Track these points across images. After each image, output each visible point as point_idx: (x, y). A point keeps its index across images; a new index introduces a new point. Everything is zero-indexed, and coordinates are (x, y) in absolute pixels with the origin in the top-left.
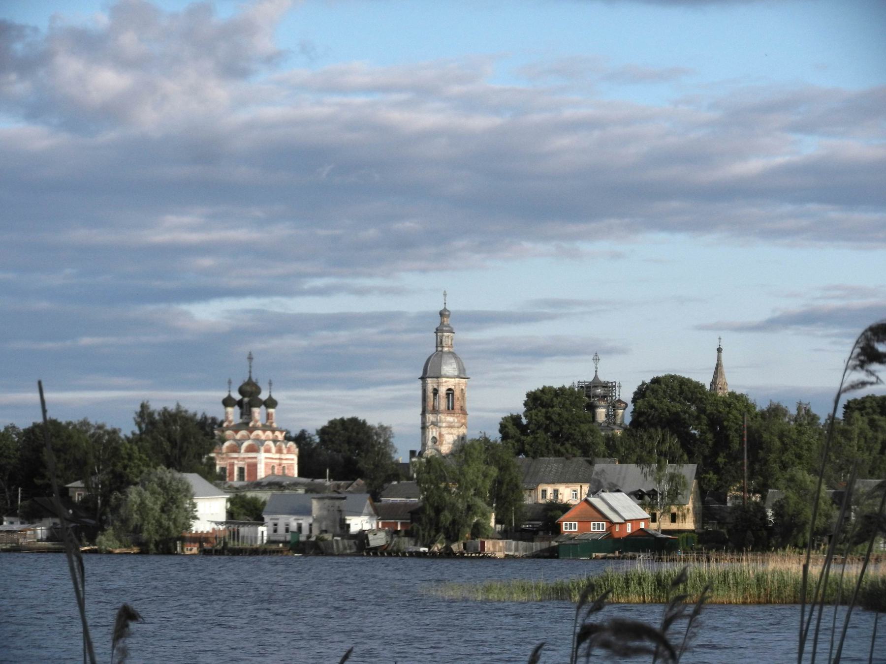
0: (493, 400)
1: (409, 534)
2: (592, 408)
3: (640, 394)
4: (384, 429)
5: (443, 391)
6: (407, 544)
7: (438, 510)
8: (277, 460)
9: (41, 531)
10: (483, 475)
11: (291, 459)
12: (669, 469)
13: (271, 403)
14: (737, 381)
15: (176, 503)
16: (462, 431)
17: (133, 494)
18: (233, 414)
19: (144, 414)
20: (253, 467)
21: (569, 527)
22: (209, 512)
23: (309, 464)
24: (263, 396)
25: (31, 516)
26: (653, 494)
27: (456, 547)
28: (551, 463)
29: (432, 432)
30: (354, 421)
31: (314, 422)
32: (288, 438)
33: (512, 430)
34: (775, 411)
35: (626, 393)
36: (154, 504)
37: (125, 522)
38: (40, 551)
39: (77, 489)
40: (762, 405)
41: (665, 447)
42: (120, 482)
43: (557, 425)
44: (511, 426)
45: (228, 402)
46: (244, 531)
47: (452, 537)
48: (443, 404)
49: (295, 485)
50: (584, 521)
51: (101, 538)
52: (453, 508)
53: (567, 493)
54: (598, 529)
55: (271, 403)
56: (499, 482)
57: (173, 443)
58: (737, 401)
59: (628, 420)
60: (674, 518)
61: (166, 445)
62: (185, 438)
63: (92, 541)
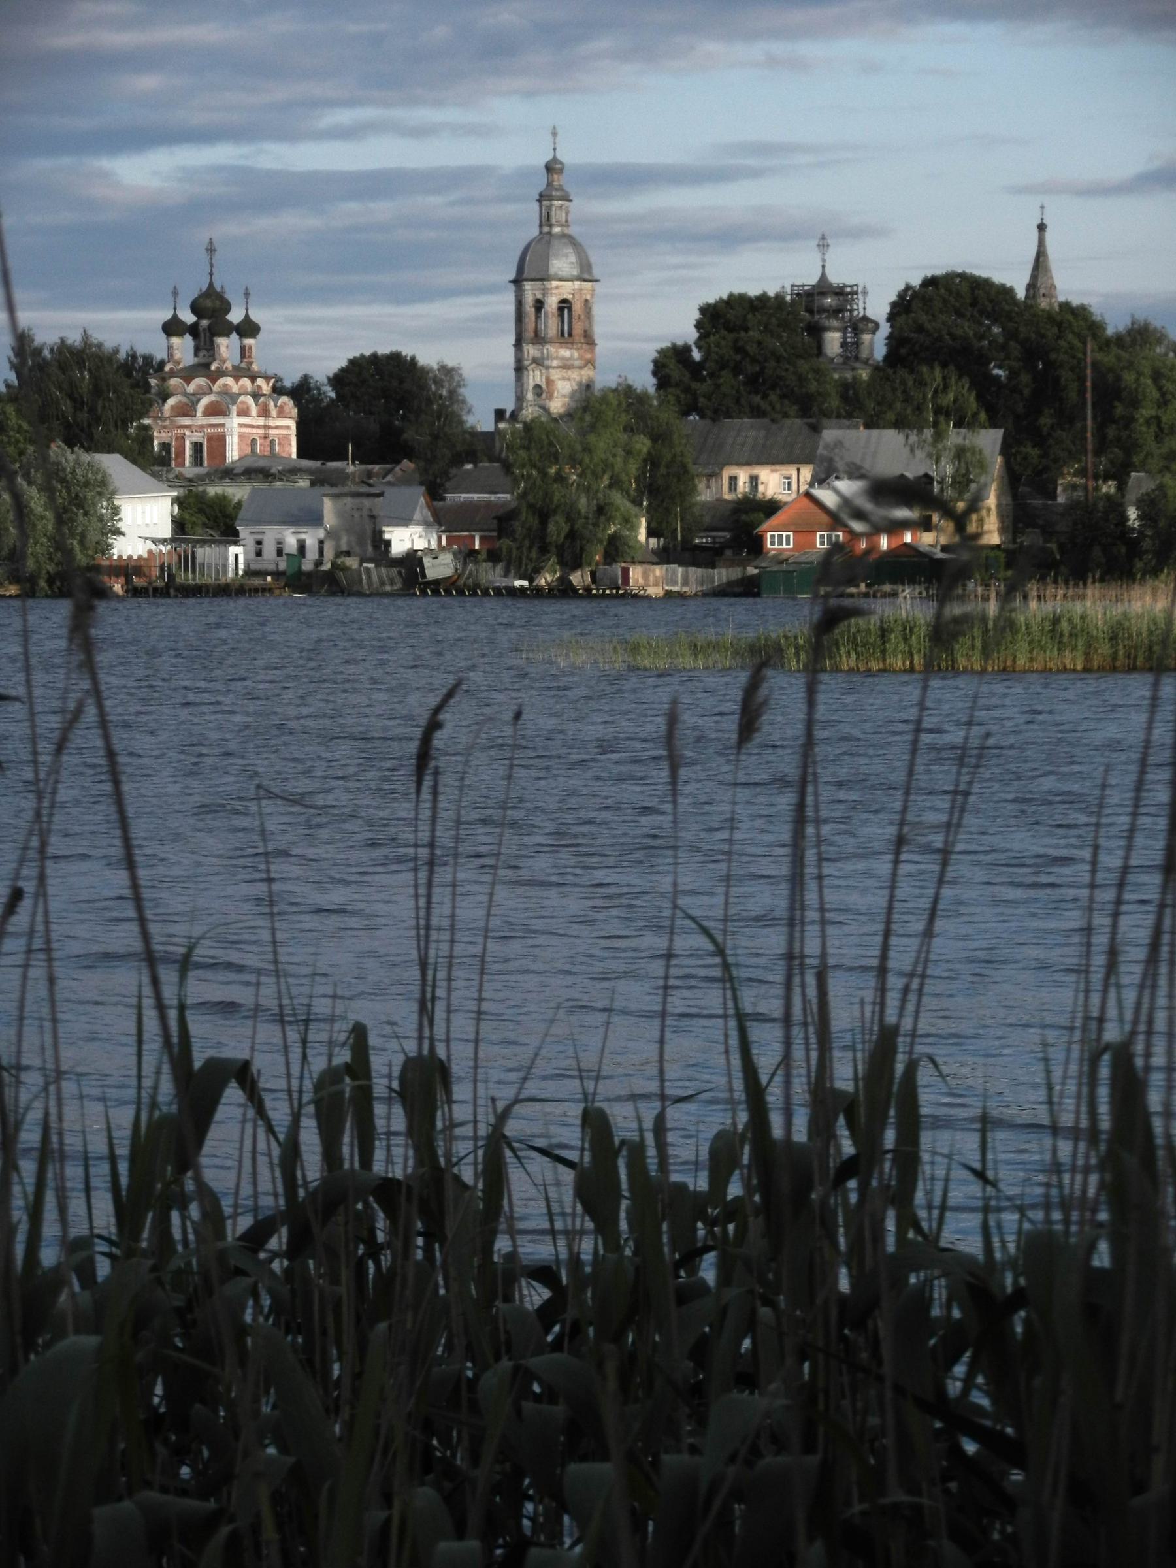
0: (642, 319)
1: (493, 556)
2: (816, 331)
3: (903, 306)
4: (448, 372)
5: (552, 303)
6: (493, 575)
8: (254, 429)
12: (955, 437)
13: (248, 329)
14: (1072, 285)
18: (183, 349)
20: (219, 442)
21: (778, 541)
22: (143, 522)
23: (316, 437)
24: (235, 316)
27: (578, 579)
28: (746, 429)
31: (324, 362)
33: (675, 371)
34: (1141, 335)
35: (877, 306)
43: (757, 361)
44: (671, 364)
45: (172, 328)
46: (204, 554)
48: (551, 327)
49: (292, 472)
50: (804, 530)
53: (773, 482)
56: (652, 460)
58: (1075, 320)
62: (97, 390)
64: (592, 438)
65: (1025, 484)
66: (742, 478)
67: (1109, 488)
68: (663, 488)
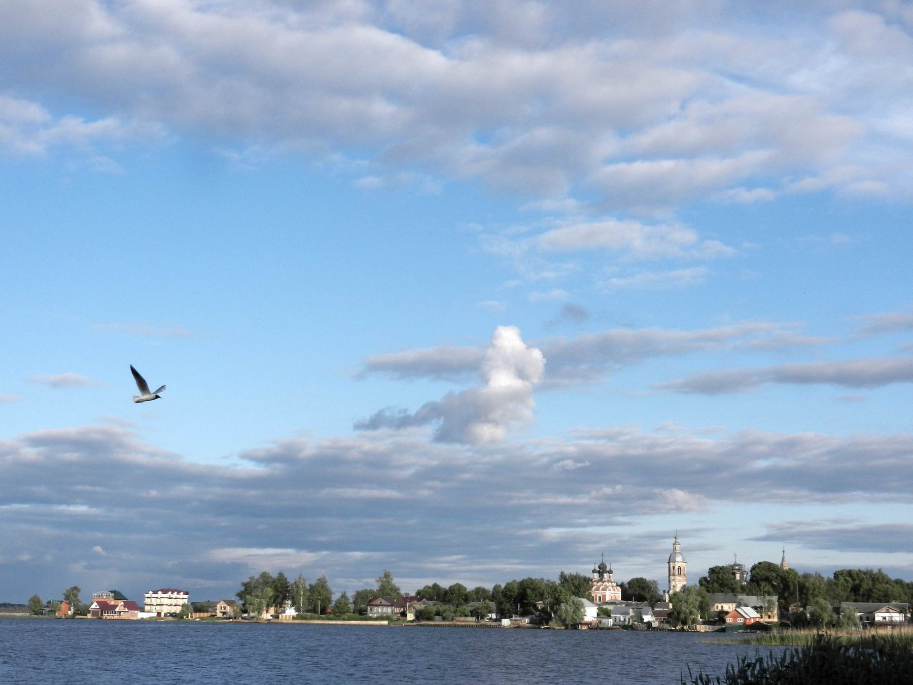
0: (695, 566)
1: (668, 622)
2: (734, 574)
3: (753, 568)
4: (655, 582)
5: (676, 567)
6: (667, 626)
7: (679, 613)
8: (613, 594)
9: (527, 620)
10: (695, 600)
11: (617, 594)
12: (768, 598)
13: (610, 572)
15: (578, 608)
16: (685, 583)
17: (563, 606)
18: (596, 576)
19: (563, 576)
20: (604, 596)
21: (729, 620)
22: (590, 613)
23: (626, 596)
24: (608, 569)
25: (524, 614)
26: (761, 607)
27: (686, 627)
28: (719, 595)
29: (673, 583)
30: (641, 579)
31: (626, 579)
32: (617, 585)
33: (704, 582)
34: (806, 576)
36: (570, 609)
37: (560, 617)
38: (528, 628)
39: (540, 604)
40: (801, 573)
41: (766, 589)
42: (557, 601)
43: (719, 581)
44: (703, 582)
45: (594, 571)
46: (604, 621)
47: (684, 623)
48: (677, 573)
49: (621, 603)
50: (735, 618)
51: (551, 623)
52: (685, 613)
53: (727, 607)
54: (740, 621)
55: (610, 572)
56: (701, 602)
57: (576, 588)
58: (791, 571)
59: (748, 579)
60: (769, 617)
61: (573, 588)
62: (579, 585)
63: (547, 624)
64: (243, 602)
65: (783, 610)
66: (718, 607)
67: (801, 609)
68: (703, 608)
